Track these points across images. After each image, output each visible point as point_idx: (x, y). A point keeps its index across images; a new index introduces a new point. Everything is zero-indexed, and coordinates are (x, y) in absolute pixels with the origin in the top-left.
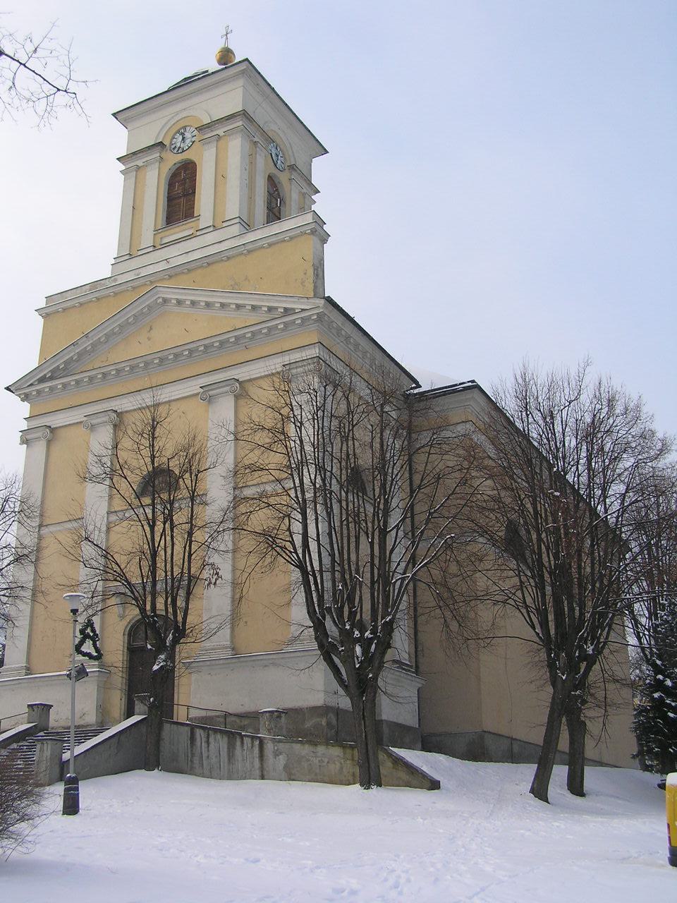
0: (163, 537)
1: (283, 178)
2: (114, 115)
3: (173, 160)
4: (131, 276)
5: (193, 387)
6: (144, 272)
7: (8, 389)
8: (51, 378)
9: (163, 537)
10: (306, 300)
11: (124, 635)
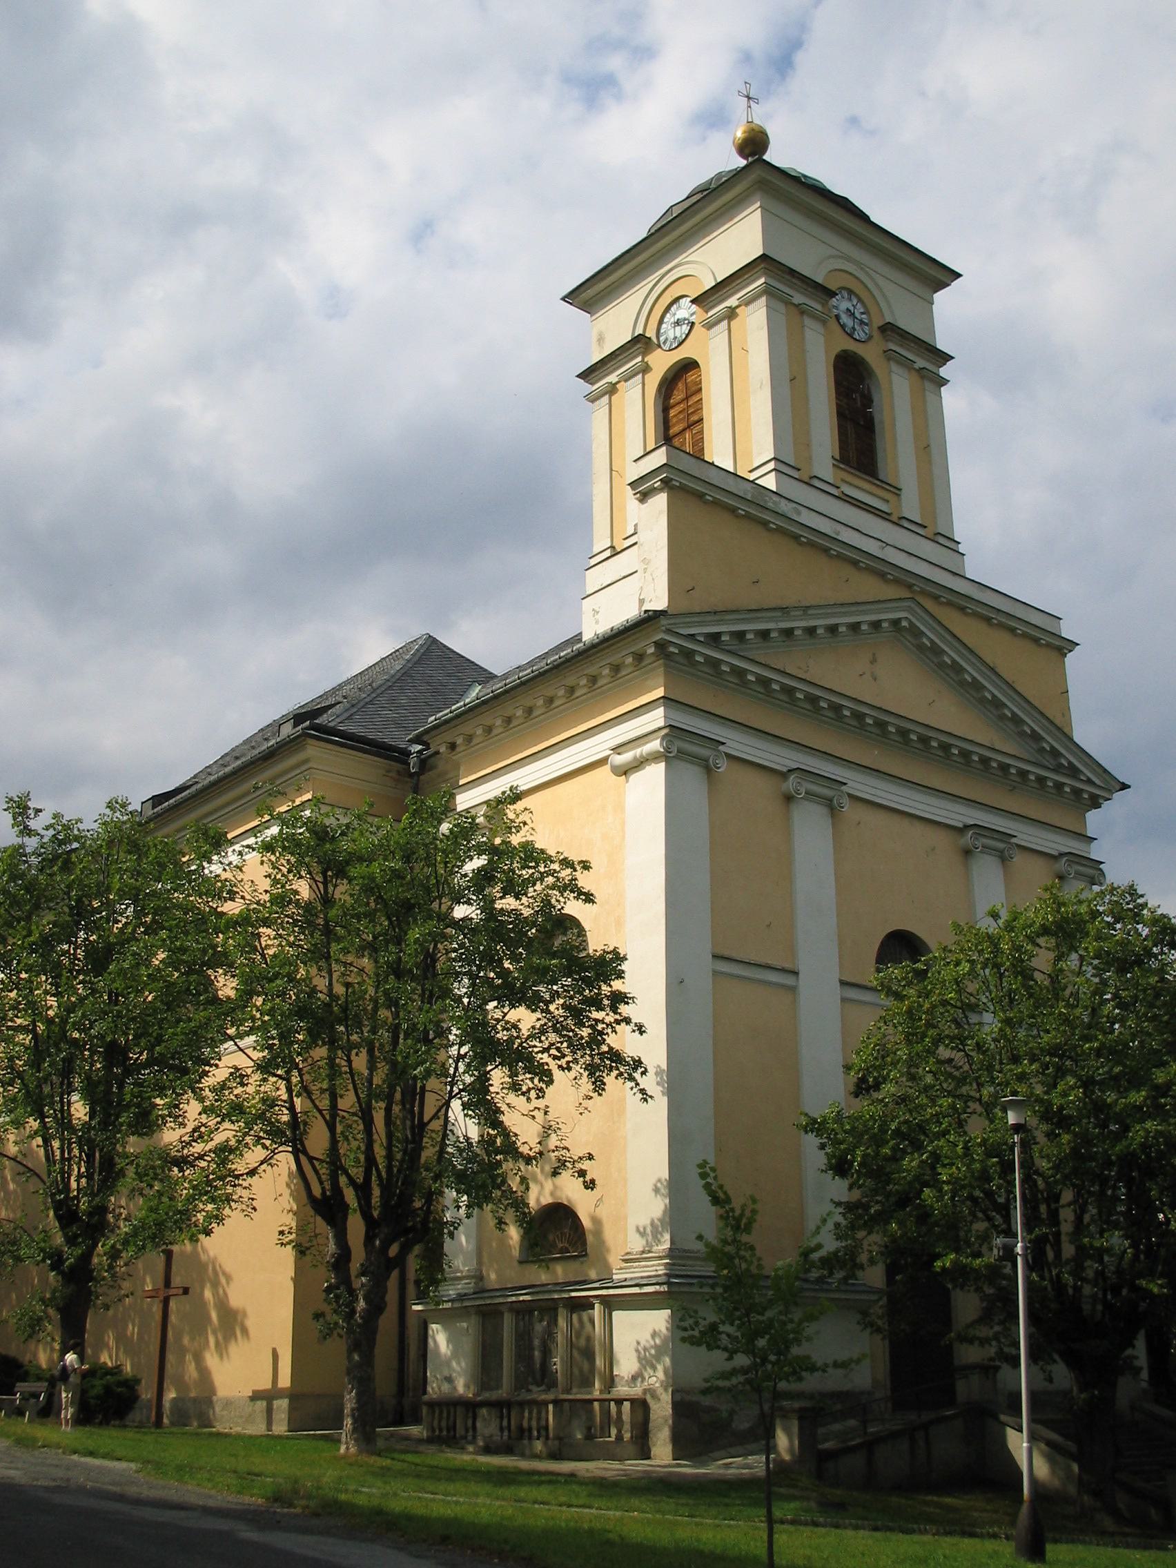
0: (1004, 745)
1: (871, 354)
2: (563, 299)
3: (661, 362)
6: (847, 536)
7: (1124, 787)
9: (1004, 745)
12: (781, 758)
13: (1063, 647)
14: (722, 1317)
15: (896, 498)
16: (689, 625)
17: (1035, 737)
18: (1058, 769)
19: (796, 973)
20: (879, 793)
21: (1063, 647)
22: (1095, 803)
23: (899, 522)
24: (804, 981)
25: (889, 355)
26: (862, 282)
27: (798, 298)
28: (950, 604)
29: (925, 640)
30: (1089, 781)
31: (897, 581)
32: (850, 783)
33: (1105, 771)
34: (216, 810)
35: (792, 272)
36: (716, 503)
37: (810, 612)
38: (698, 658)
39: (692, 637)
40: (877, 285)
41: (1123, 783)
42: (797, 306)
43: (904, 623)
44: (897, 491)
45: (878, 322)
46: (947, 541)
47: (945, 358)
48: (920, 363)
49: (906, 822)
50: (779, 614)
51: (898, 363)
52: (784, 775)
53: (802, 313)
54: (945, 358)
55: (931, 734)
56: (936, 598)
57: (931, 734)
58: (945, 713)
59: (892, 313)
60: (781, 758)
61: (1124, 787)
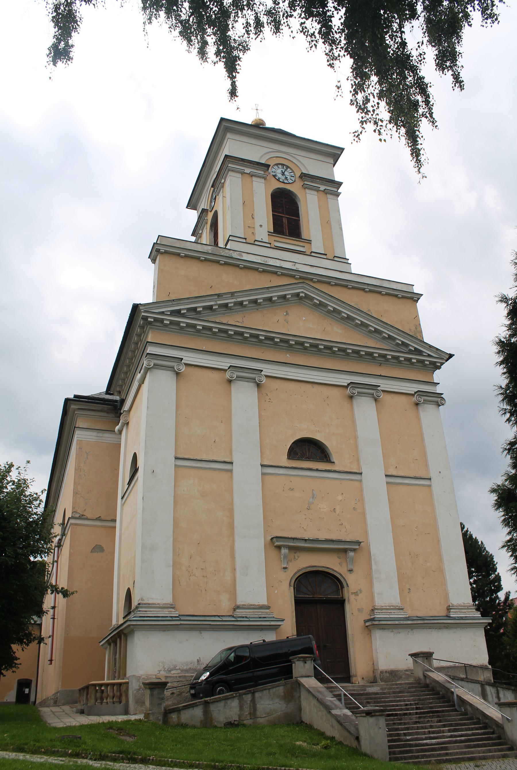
0: (234, 320)
1: (296, 188)
4: (278, 263)
5: (344, 380)
8: (183, 316)
10: (435, 350)
11: (290, 586)
12: (224, 363)
13: (414, 298)
14: (30, 628)
15: (309, 244)
16: (161, 307)
17: (390, 338)
18: (410, 352)
19: (232, 463)
20: (289, 374)
21: (414, 298)
22: (436, 367)
23: (311, 254)
24: (236, 467)
25: (305, 187)
26: (285, 158)
27: (248, 170)
28: (319, 281)
29: (315, 301)
30: (429, 356)
31: (283, 275)
32: (184, 358)
33: (437, 349)
34: (317, 470)
35: (243, 160)
36: (186, 256)
37: (235, 295)
38: (413, 361)
39: (163, 313)
40: (298, 160)
41: (450, 354)
42: (249, 174)
43: (301, 295)
44: (309, 242)
45: (298, 174)
46: (344, 260)
47: (340, 184)
48: (322, 188)
49: (310, 386)
50: (216, 297)
51: (331, 194)
52: (346, 387)
53: (252, 176)
54: (340, 184)
55: (348, 347)
56: (311, 280)
57: (348, 347)
58: (336, 333)
59: (307, 170)
60: (224, 363)
61: (451, 356)
